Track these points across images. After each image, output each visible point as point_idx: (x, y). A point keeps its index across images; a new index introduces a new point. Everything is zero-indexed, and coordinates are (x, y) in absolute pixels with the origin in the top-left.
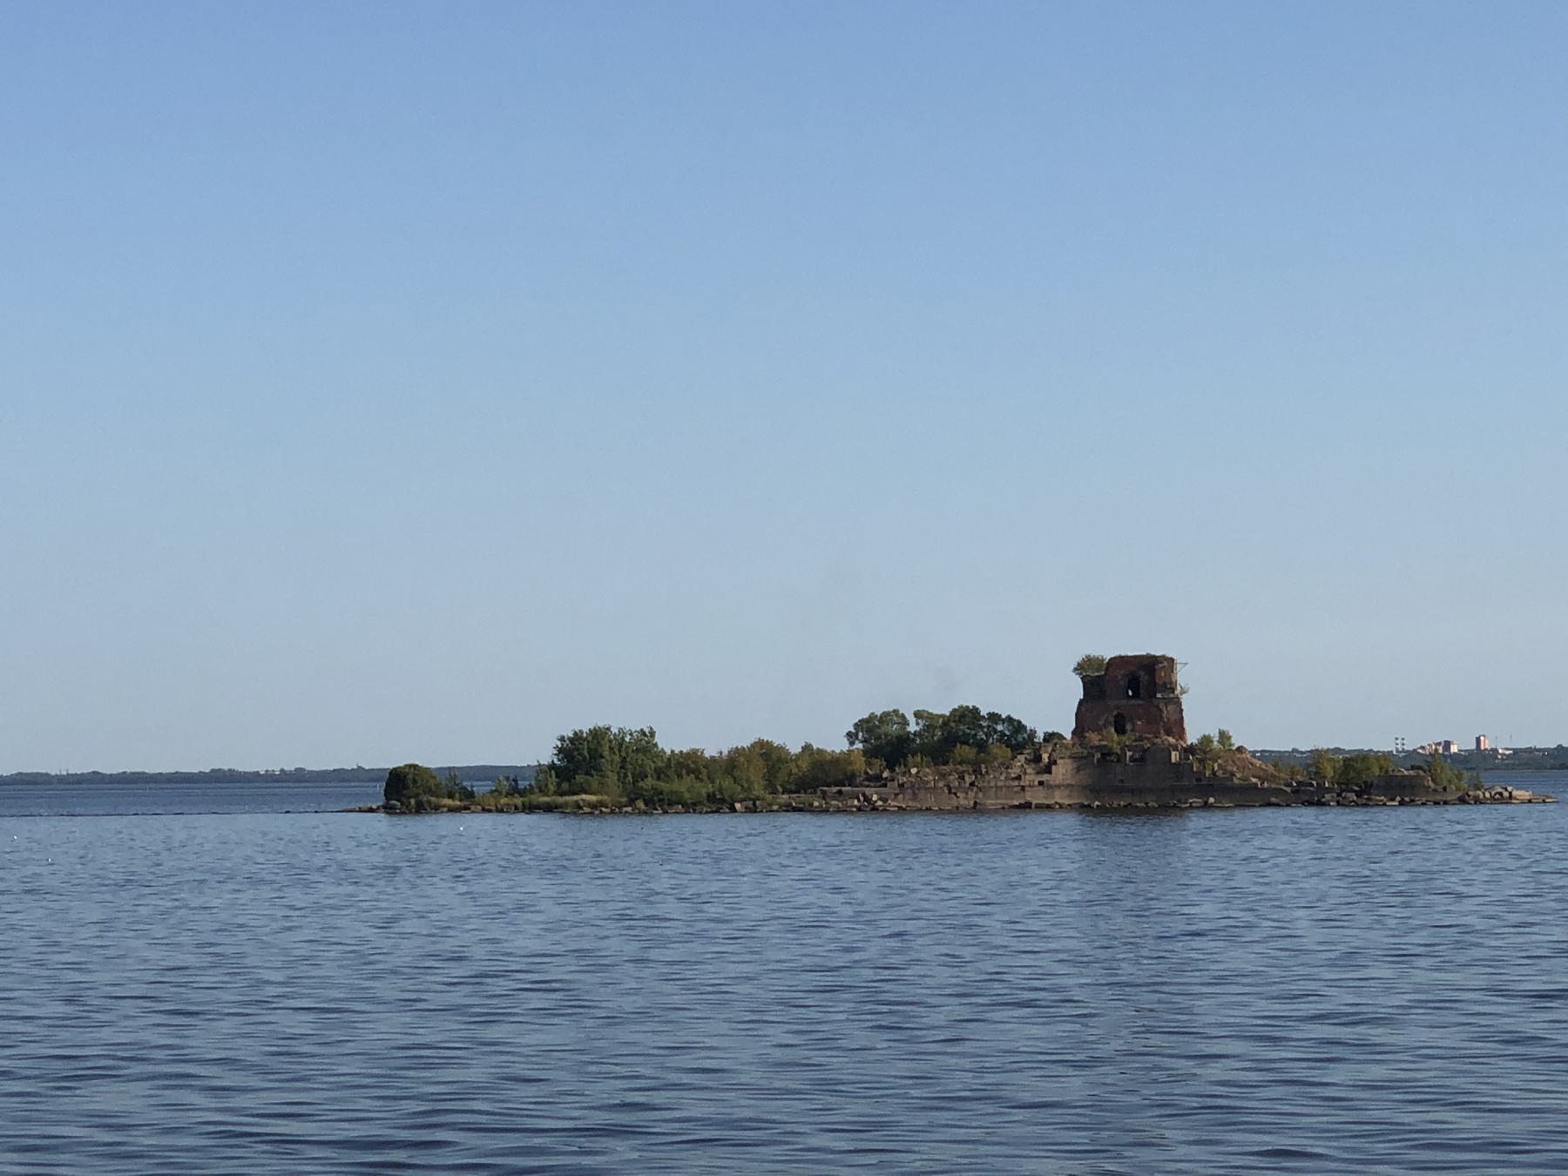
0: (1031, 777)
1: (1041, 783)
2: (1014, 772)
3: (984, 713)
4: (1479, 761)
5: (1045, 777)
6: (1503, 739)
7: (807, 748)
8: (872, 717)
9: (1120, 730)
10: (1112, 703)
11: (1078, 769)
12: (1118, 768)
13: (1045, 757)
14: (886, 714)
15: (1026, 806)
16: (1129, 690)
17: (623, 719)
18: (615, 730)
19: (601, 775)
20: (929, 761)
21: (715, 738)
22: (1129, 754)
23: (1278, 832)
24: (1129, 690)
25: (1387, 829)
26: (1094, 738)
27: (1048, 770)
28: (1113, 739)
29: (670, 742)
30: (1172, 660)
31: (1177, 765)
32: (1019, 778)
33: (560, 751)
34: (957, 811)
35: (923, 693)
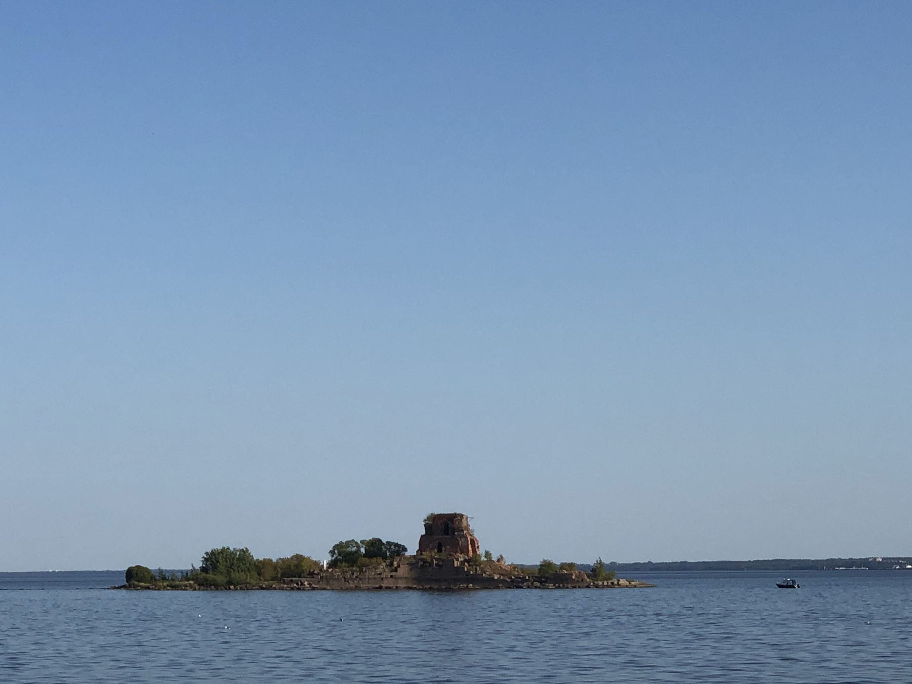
0: (388, 573)
1: (392, 576)
2: (378, 571)
3: (384, 542)
4: (615, 569)
5: (394, 574)
6: (621, 560)
7: (207, 553)
8: (341, 543)
9: (440, 551)
10: (435, 537)
11: (411, 570)
12: (430, 569)
13: (395, 564)
14: (348, 542)
15: (380, 588)
16: (445, 530)
17: (234, 544)
18: (232, 549)
19: (225, 571)
20: (361, 564)
21: (532, 559)
22: (435, 562)
23: (530, 599)
24: (445, 530)
25: (574, 599)
26: (426, 555)
27: (396, 570)
28: (435, 553)
29: (258, 554)
30: (462, 516)
31: (458, 567)
32: (380, 574)
33: (206, 560)
34: (351, 589)
35: (360, 532)
